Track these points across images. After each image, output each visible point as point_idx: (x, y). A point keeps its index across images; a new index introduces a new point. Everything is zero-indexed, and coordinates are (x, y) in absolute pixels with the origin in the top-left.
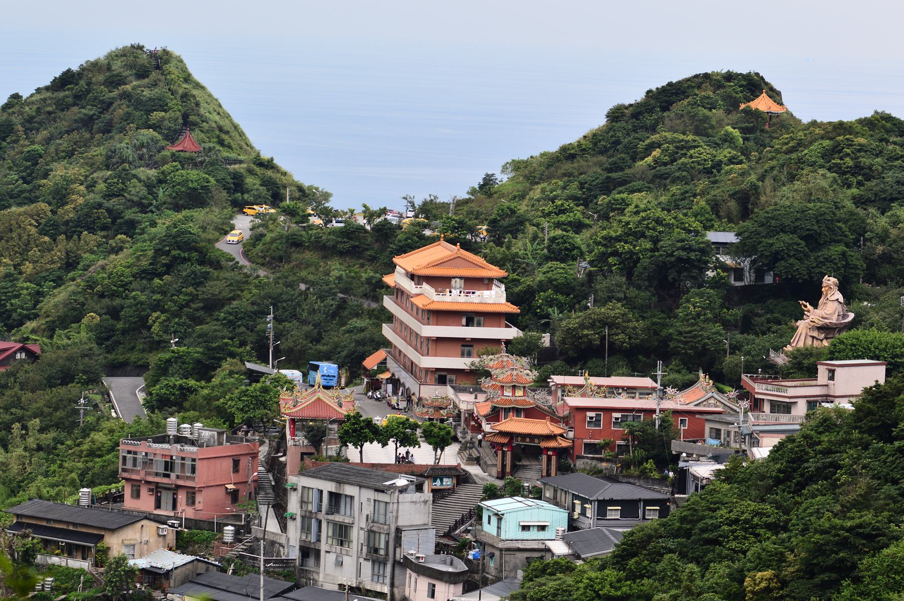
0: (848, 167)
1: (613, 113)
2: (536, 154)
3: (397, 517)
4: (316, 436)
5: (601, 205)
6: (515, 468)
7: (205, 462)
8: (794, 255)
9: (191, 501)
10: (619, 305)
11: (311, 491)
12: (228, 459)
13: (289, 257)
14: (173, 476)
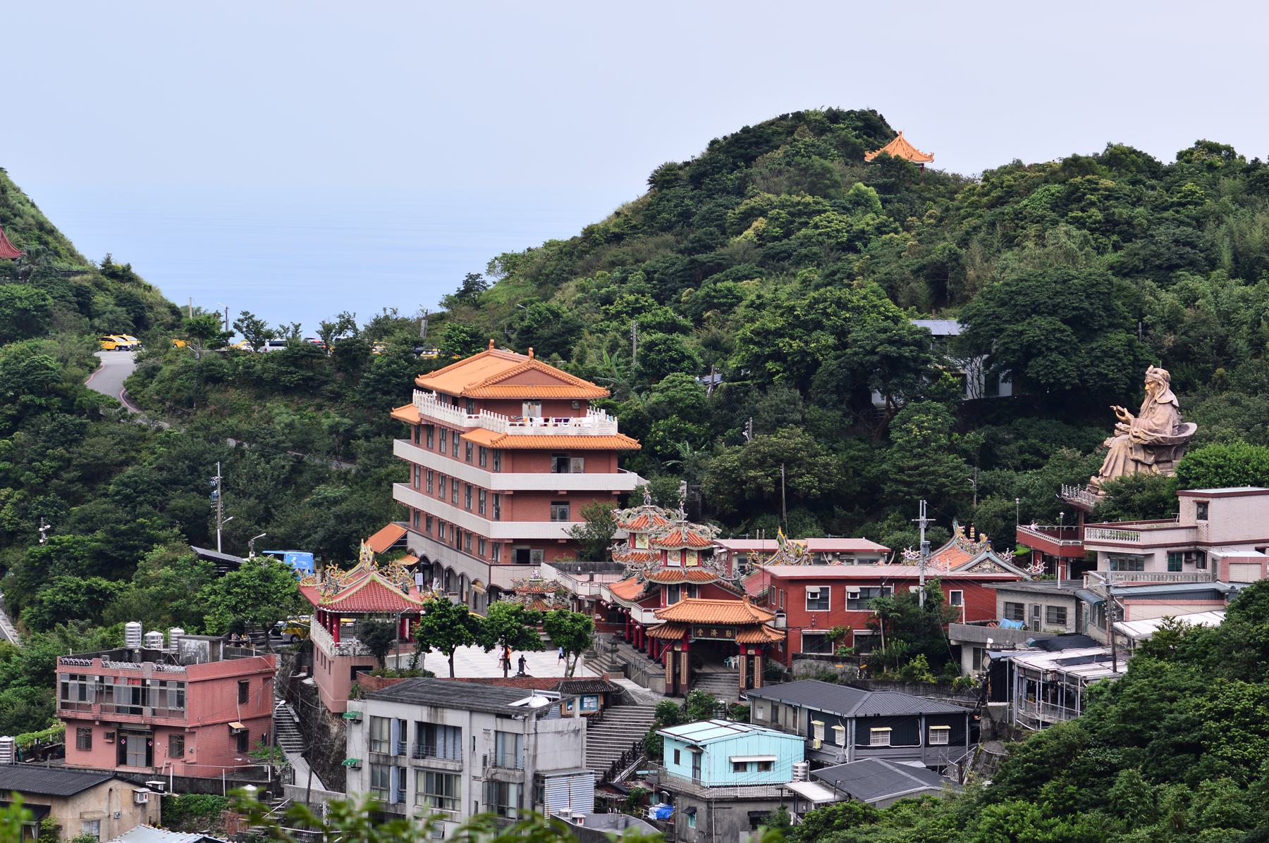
0: (1095, 222)
1: (662, 175)
2: (537, 244)
3: (535, 757)
4: (379, 637)
5: (686, 303)
6: (694, 679)
7: (199, 687)
8: (1057, 348)
9: (177, 749)
10: (799, 431)
11: (385, 723)
12: (231, 681)
13: (205, 399)
14: (147, 711)
